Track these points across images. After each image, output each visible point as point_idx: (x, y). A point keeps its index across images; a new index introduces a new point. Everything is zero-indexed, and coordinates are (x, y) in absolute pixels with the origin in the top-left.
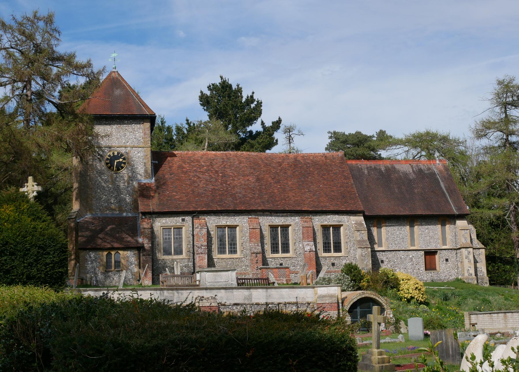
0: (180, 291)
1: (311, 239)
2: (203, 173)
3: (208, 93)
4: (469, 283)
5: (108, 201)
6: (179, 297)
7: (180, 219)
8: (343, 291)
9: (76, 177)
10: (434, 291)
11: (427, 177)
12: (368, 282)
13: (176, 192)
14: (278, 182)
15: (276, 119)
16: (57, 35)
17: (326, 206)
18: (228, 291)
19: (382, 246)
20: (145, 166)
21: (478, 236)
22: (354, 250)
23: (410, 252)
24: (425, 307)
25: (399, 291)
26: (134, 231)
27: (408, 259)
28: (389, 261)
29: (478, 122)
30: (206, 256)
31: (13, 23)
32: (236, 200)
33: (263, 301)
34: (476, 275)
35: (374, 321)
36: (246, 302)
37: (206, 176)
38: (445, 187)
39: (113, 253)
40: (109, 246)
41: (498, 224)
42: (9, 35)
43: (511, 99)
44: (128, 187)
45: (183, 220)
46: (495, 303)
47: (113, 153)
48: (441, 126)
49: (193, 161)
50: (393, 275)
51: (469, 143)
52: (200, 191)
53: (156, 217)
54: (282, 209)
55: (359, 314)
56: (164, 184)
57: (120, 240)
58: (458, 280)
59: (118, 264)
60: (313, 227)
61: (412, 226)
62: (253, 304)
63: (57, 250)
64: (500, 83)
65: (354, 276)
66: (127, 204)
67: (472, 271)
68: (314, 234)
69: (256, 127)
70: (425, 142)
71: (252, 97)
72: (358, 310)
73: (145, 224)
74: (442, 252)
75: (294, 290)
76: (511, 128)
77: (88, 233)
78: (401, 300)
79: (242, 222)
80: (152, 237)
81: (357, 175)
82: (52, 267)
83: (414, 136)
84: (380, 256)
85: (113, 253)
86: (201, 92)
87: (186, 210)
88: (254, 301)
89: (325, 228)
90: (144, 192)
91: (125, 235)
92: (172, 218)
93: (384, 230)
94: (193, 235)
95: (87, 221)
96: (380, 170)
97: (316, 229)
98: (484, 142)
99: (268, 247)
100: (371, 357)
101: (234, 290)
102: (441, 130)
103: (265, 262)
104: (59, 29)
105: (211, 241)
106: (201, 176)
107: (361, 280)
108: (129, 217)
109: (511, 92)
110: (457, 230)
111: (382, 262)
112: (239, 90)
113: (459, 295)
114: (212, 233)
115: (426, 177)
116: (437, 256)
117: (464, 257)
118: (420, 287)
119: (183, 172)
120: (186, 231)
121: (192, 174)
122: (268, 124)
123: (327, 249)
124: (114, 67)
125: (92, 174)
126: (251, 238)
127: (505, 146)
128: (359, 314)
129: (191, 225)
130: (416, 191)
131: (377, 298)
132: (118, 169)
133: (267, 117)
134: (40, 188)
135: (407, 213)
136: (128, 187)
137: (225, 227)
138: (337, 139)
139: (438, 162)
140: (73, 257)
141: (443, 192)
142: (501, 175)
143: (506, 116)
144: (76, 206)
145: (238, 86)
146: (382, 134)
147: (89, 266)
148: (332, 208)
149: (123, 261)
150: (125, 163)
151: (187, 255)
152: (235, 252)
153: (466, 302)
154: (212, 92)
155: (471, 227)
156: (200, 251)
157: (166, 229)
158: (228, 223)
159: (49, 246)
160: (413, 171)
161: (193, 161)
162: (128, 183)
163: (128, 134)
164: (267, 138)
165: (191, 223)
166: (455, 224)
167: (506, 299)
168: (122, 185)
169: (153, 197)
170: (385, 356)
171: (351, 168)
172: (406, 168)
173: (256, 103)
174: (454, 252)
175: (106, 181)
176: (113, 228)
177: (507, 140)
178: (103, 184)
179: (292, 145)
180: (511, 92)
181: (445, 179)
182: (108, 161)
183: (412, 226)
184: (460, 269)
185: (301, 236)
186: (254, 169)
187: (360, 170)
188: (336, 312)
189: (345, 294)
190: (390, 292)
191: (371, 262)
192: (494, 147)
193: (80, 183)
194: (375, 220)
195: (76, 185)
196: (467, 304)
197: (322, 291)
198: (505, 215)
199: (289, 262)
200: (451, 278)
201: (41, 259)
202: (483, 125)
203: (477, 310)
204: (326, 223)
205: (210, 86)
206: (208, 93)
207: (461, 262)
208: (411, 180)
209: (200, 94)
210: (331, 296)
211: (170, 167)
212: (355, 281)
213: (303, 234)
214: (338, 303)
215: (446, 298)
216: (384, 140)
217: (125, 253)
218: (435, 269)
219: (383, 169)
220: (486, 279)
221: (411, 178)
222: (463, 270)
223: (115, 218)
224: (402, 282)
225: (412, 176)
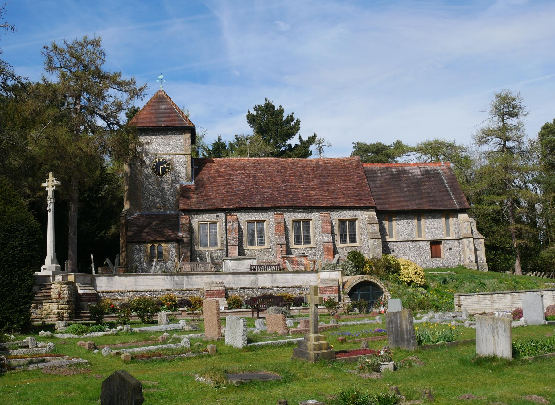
0: (190, 276)
1: (330, 232)
2: (237, 176)
3: (255, 113)
4: (470, 269)
5: (154, 201)
6: (189, 282)
7: (215, 215)
9: (127, 181)
10: (435, 276)
11: (433, 177)
12: (371, 267)
13: (213, 193)
14: (302, 183)
15: (312, 135)
16: (102, 57)
17: (342, 203)
18: (235, 276)
19: (393, 238)
20: (186, 170)
21: (479, 229)
22: (367, 241)
23: (417, 243)
24: (423, 289)
25: (400, 275)
26: (176, 226)
27: (416, 248)
28: (399, 250)
29: (479, 130)
31: (65, 47)
32: (264, 199)
33: (268, 285)
34: (476, 262)
35: (311, 302)
36: (253, 286)
37: (239, 179)
38: (449, 185)
39: (156, 245)
40: (152, 239)
41: (498, 218)
42: (59, 56)
43: (507, 110)
44: (171, 189)
45: (218, 216)
46: (490, 286)
47: (159, 160)
48: (447, 136)
49: (228, 166)
50: (394, 261)
52: (233, 191)
53: (194, 214)
54: (304, 205)
55: (358, 296)
56: (202, 186)
57: (162, 234)
58: (460, 266)
59: (160, 254)
60: (331, 221)
61: (419, 219)
62: (259, 288)
63: (26, 233)
64: (498, 96)
65: (358, 262)
66: (170, 203)
67: (473, 258)
68: (332, 227)
70: (434, 149)
71: (292, 116)
72: (358, 292)
73: (184, 221)
74: (446, 242)
75: (298, 274)
76: (507, 134)
77: (135, 228)
78: (402, 283)
79: (269, 217)
80: (191, 231)
81: (370, 176)
82: (20, 250)
83: (425, 144)
84: (391, 246)
85: (156, 245)
86: (249, 112)
87: (220, 207)
88: (260, 285)
89: (342, 222)
90: (185, 192)
91: (166, 230)
92: (208, 215)
93: (394, 223)
94: (226, 229)
95: (136, 218)
96: (392, 171)
97: (334, 223)
98: (486, 148)
99: (291, 239)
100: (307, 342)
101: (242, 275)
102: (447, 137)
103: (288, 251)
104: (105, 52)
105: (242, 234)
106: (235, 179)
107: (363, 265)
108: (173, 214)
109: (507, 103)
110: (460, 222)
112: (281, 111)
113: (457, 279)
114: (243, 227)
115: (431, 177)
116: (442, 246)
117: (466, 246)
118: (419, 272)
119: (219, 175)
120: (221, 225)
121: (227, 177)
122: (305, 138)
123: (343, 240)
124: (161, 86)
125: (141, 178)
126: (276, 231)
127: (503, 150)
128: (358, 296)
129: (224, 221)
130: (423, 189)
131: (376, 282)
132: (163, 174)
133: (304, 133)
134: (59, 183)
135: (415, 208)
136: (171, 189)
137: (254, 222)
138: (360, 148)
139: (442, 164)
140: (124, 249)
141: (447, 190)
142: (498, 176)
143: (504, 124)
144: (127, 206)
145: (281, 107)
146: (398, 143)
147: (135, 256)
148: (347, 205)
149: (164, 252)
150: (168, 168)
151: (221, 247)
153: (463, 285)
154: (257, 112)
155: (472, 220)
156: (231, 243)
157: (203, 224)
158: (257, 219)
159: (18, 230)
160: (421, 172)
161: (228, 166)
162: (172, 186)
163: (171, 143)
164: (303, 150)
165: (224, 218)
166: (457, 217)
167: (500, 282)
168: (166, 187)
170: (323, 342)
171: (366, 171)
172: (415, 170)
173: (295, 121)
174: (457, 242)
175: (152, 184)
176: (157, 224)
177: (504, 145)
178: (150, 186)
179: (322, 155)
180: (507, 103)
181: (449, 178)
182: (154, 167)
183: (419, 219)
184: (462, 257)
185: (321, 229)
186: (281, 172)
187: (374, 172)
188: (337, 295)
189: (346, 279)
190: (391, 276)
192: (493, 152)
193: (130, 186)
194: (385, 215)
195: (126, 188)
196: (464, 287)
197: (325, 275)
198: (503, 210)
199: (310, 252)
200: (454, 265)
201: (8, 242)
202: (484, 133)
203: (473, 292)
204: (342, 218)
205: (256, 107)
206: (255, 113)
207: (463, 251)
208: (418, 180)
209: (247, 114)
210: (333, 280)
211: (208, 171)
212: (358, 266)
213: (322, 227)
214: (339, 286)
215: (445, 282)
216: (400, 148)
217: (167, 245)
218: (440, 257)
219: (394, 171)
220: (486, 265)
221: (419, 178)
222: (465, 258)
223: (161, 215)
224: (402, 267)
225: (420, 176)
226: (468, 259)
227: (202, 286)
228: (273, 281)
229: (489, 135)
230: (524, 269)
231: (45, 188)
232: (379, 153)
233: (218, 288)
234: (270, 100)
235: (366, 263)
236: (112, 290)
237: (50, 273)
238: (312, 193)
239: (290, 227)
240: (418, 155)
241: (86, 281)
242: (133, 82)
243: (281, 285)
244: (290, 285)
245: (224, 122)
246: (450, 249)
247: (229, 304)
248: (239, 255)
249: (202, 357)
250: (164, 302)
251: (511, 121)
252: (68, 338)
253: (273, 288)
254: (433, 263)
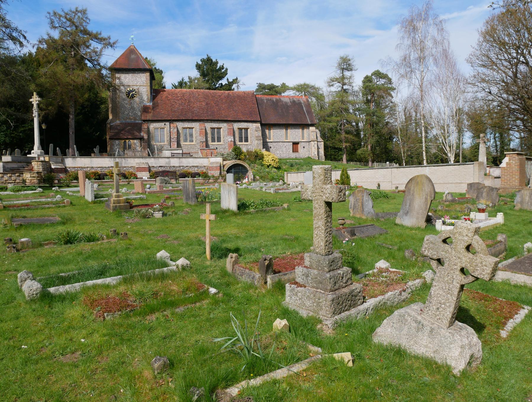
2: (178, 100)
8: (224, 160)
16: (88, 21)
30: (176, 143)
31: (62, 14)
33: (177, 165)
36: (167, 165)
43: (345, 66)
45: (165, 124)
51: (324, 89)
56: (157, 106)
58: (309, 157)
59: (130, 147)
64: (341, 58)
67: (316, 153)
68: (234, 132)
69: (224, 82)
70: (303, 88)
73: (145, 126)
77: (116, 131)
79: (196, 126)
80: (148, 132)
83: (298, 86)
84: (270, 145)
85: (127, 141)
88: (172, 165)
89: (240, 129)
90: (145, 109)
91: (135, 132)
93: (272, 131)
99: (210, 139)
103: (207, 146)
112: (217, 63)
133: (230, 76)
135: (284, 123)
137: (187, 128)
144: (111, 117)
148: (244, 119)
152: (193, 141)
155: (317, 131)
169: (151, 112)
174: (308, 143)
177: (343, 88)
187: (262, 100)
189: (225, 162)
194: (266, 126)
202: (331, 80)
204: (240, 127)
206: (200, 63)
210: (217, 163)
212: (237, 155)
216: (284, 87)
219: (274, 100)
220: (324, 157)
225: (289, 104)
226: (313, 153)
227: (134, 165)
228: (180, 163)
229: (333, 81)
230: (348, 161)
231: (31, 102)
232: (272, 89)
233: (144, 166)
234: (209, 55)
235: (242, 153)
236: (76, 166)
237: (36, 156)
238: (223, 112)
239: (209, 131)
240: (294, 92)
241: (58, 161)
242: (109, 38)
243: (185, 165)
244: (191, 165)
245: (178, 69)
247: (151, 176)
248: (178, 147)
249: (59, 207)
250: (108, 174)
251: (347, 74)
252: (7, 194)
253: (180, 167)
254: (294, 155)
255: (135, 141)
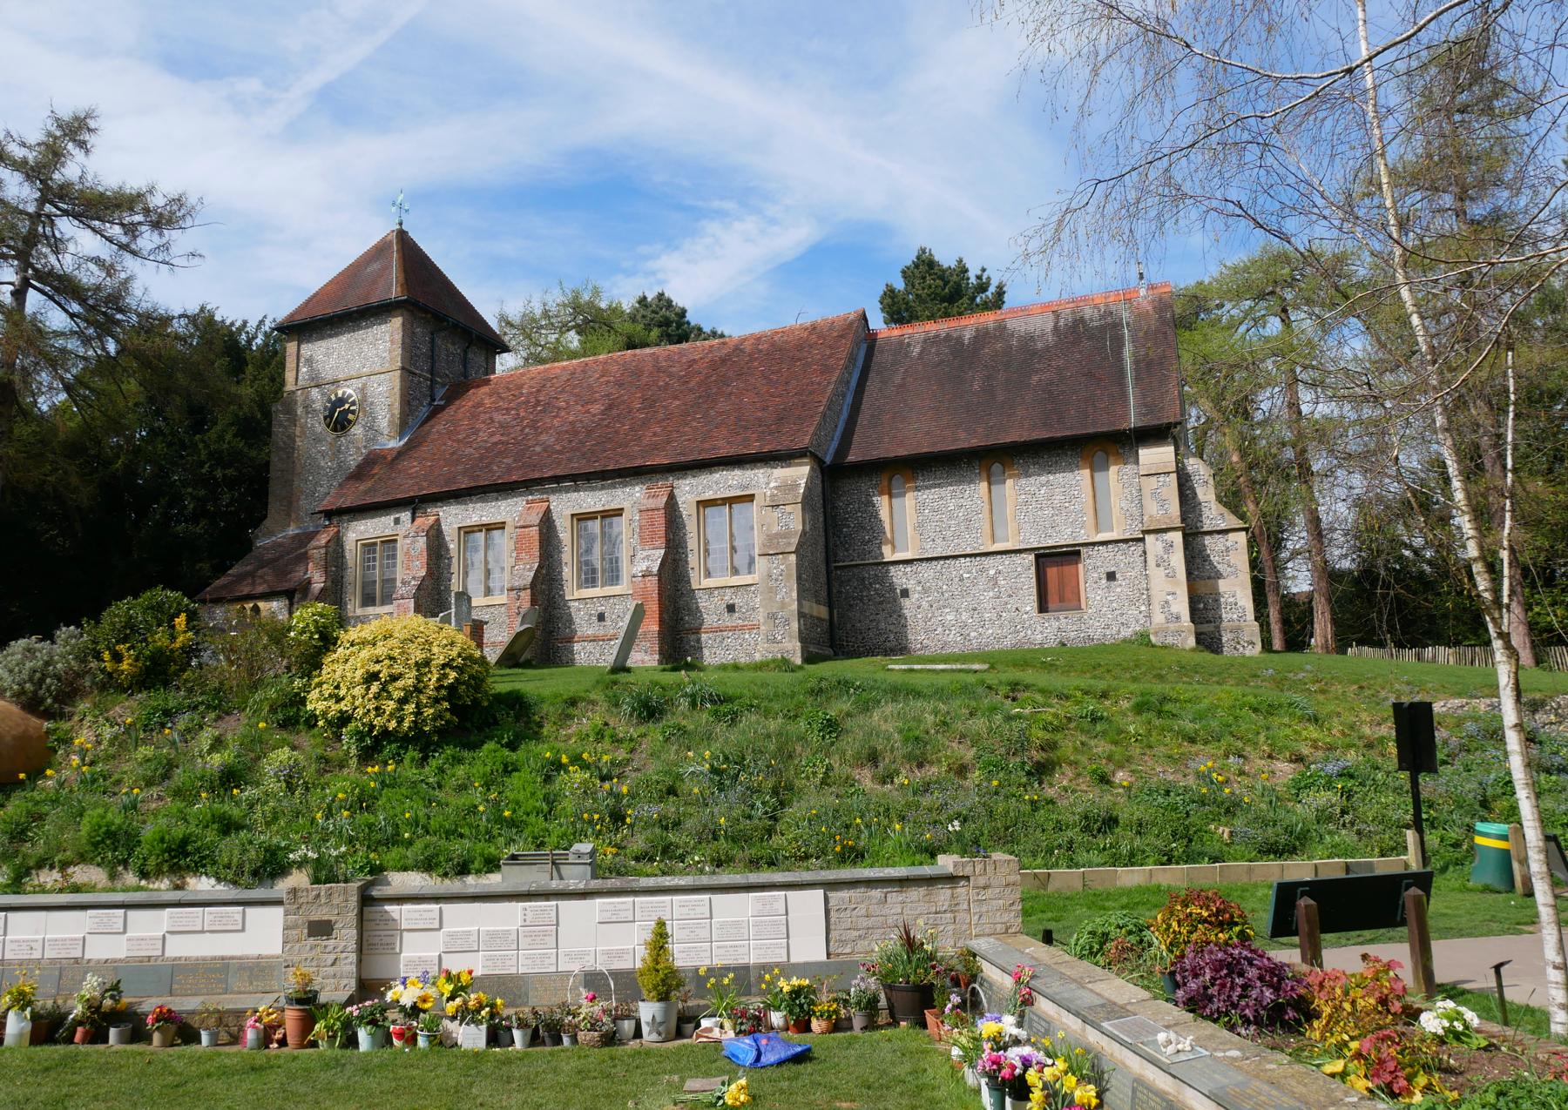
4: (1165, 647)
28: (926, 591)
45: (397, 521)
67: (1181, 606)
74: (1094, 552)
111: (905, 593)
158: (485, 520)
174: (1136, 549)
191: (795, 595)
239: (564, 532)
246: (1111, 576)
251: (1481, 133)
254: (1045, 631)
255: (274, 604)
